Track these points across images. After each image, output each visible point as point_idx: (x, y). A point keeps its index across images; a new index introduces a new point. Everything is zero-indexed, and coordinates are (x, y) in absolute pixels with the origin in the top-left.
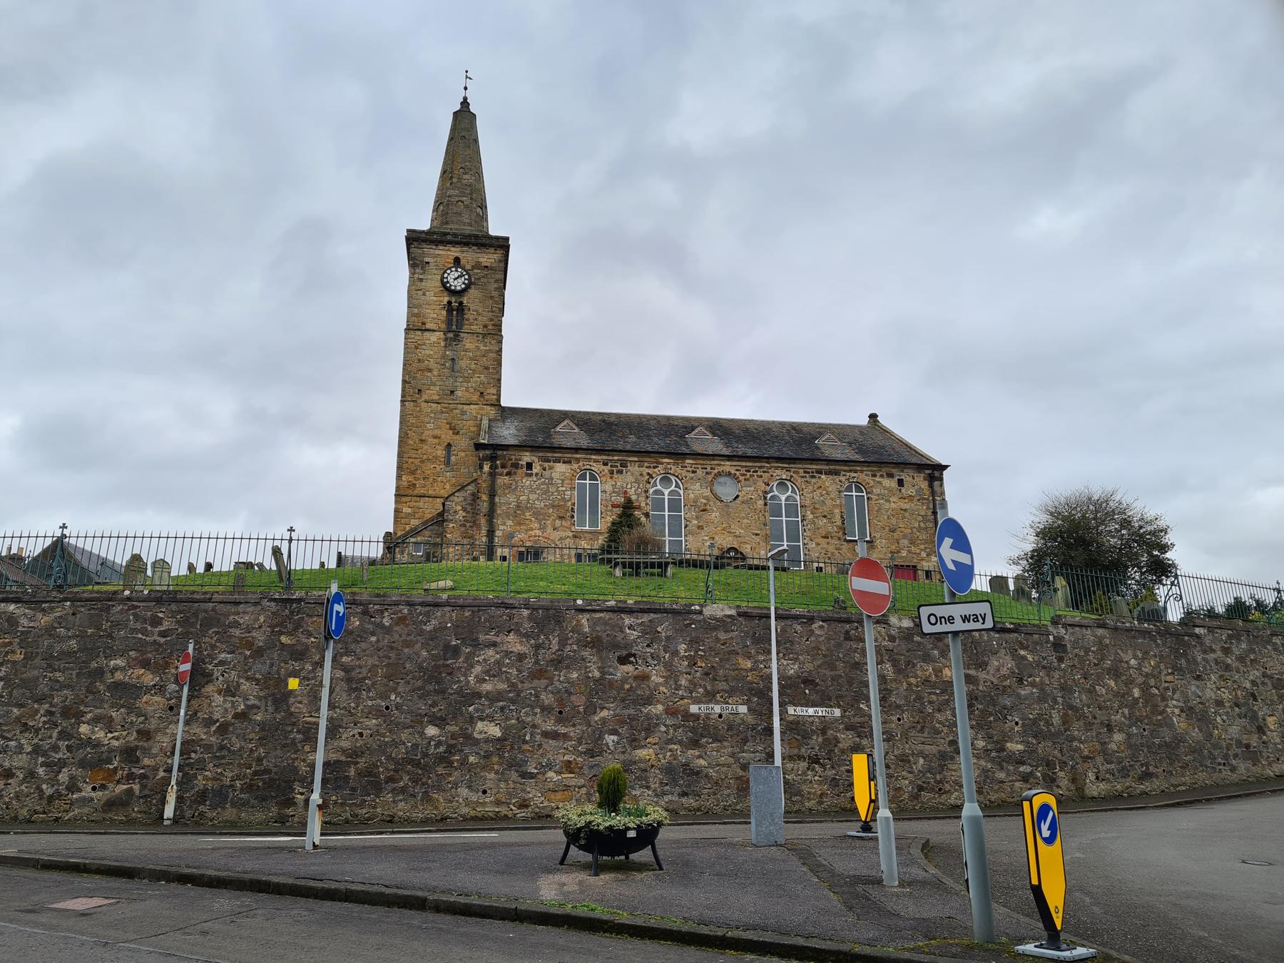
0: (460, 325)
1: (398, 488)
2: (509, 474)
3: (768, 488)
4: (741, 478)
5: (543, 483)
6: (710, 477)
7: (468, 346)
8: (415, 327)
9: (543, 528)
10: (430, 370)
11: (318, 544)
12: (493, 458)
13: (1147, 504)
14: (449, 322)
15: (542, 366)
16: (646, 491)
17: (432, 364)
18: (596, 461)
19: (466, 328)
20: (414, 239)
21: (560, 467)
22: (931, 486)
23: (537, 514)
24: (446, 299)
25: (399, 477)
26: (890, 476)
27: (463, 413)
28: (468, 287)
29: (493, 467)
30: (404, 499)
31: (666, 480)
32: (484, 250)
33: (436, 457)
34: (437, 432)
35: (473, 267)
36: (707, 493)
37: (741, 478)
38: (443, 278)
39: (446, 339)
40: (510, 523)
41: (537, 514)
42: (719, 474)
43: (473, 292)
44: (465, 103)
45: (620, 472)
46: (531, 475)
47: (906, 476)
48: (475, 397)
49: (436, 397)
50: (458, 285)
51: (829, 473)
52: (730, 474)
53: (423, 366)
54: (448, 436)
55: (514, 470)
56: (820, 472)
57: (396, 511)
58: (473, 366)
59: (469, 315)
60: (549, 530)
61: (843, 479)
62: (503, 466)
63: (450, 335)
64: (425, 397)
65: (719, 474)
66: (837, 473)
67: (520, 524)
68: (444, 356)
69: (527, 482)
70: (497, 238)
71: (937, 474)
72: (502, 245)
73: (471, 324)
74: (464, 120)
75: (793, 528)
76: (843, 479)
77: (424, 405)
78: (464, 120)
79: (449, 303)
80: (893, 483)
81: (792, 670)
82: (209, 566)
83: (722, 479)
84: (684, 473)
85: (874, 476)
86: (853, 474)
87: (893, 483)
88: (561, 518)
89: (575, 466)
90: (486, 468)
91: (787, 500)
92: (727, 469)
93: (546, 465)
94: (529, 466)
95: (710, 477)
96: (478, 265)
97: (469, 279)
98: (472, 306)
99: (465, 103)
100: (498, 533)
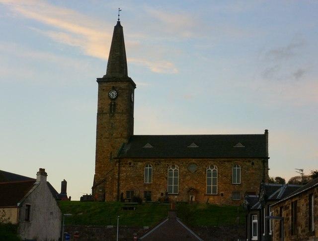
0: (114, 110)
10: (105, 127)
12: (119, 162)
13: (282, 177)
14: (111, 109)
15: (148, 121)
21: (140, 164)
22: (264, 164)
26: (249, 161)
29: (119, 165)
31: (173, 167)
39: (110, 116)
42: (191, 164)
43: (119, 98)
44: (119, 23)
45: (159, 164)
47: (255, 161)
51: (228, 161)
52: (194, 163)
59: (118, 107)
61: (233, 163)
66: (230, 161)
71: (266, 160)
75: (214, 180)
77: (103, 139)
79: (111, 103)
80: (250, 164)
81: (123, 237)
82: (70, 197)
83: (191, 165)
85: (244, 162)
87: (250, 164)
90: (117, 165)
94: (130, 164)
99: (119, 23)
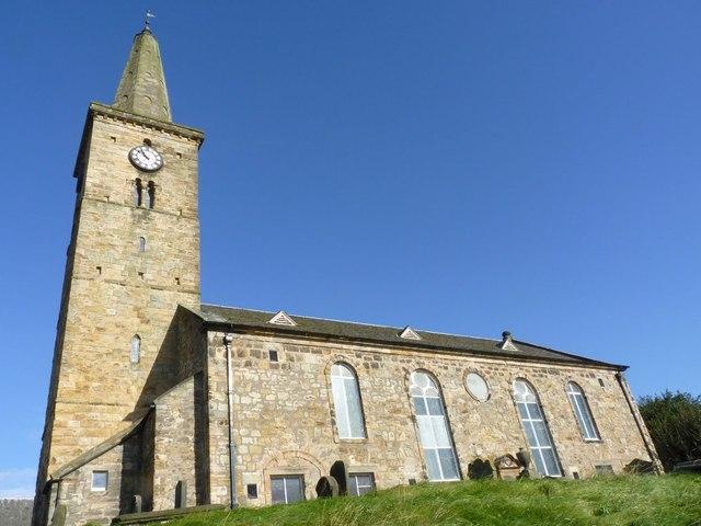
5: (293, 378)
9: (300, 440)
10: (113, 246)
16: (407, 390)
17: (116, 240)
18: (348, 351)
23: (290, 418)
26: (593, 376)
27: (153, 299)
35: (165, 152)
39: (133, 216)
40: (256, 433)
41: (290, 418)
43: (164, 173)
45: (375, 366)
46: (276, 367)
48: (171, 282)
50: (150, 164)
54: (134, 323)
55: (254, 359)
58: (166, 248)
62: (241, 355)
63: (140, 212)
64: (106, 274)
67: (270, 435)
68: (132, 234)
69: (274, 376)
70: (38, 491)
77: (104, 286)
79: (138, 181)
88: (320, 424)
93: (293, 354)
94: (274, 355)
95: (461, 374)
96: (170, 150)
100: (243, 449)
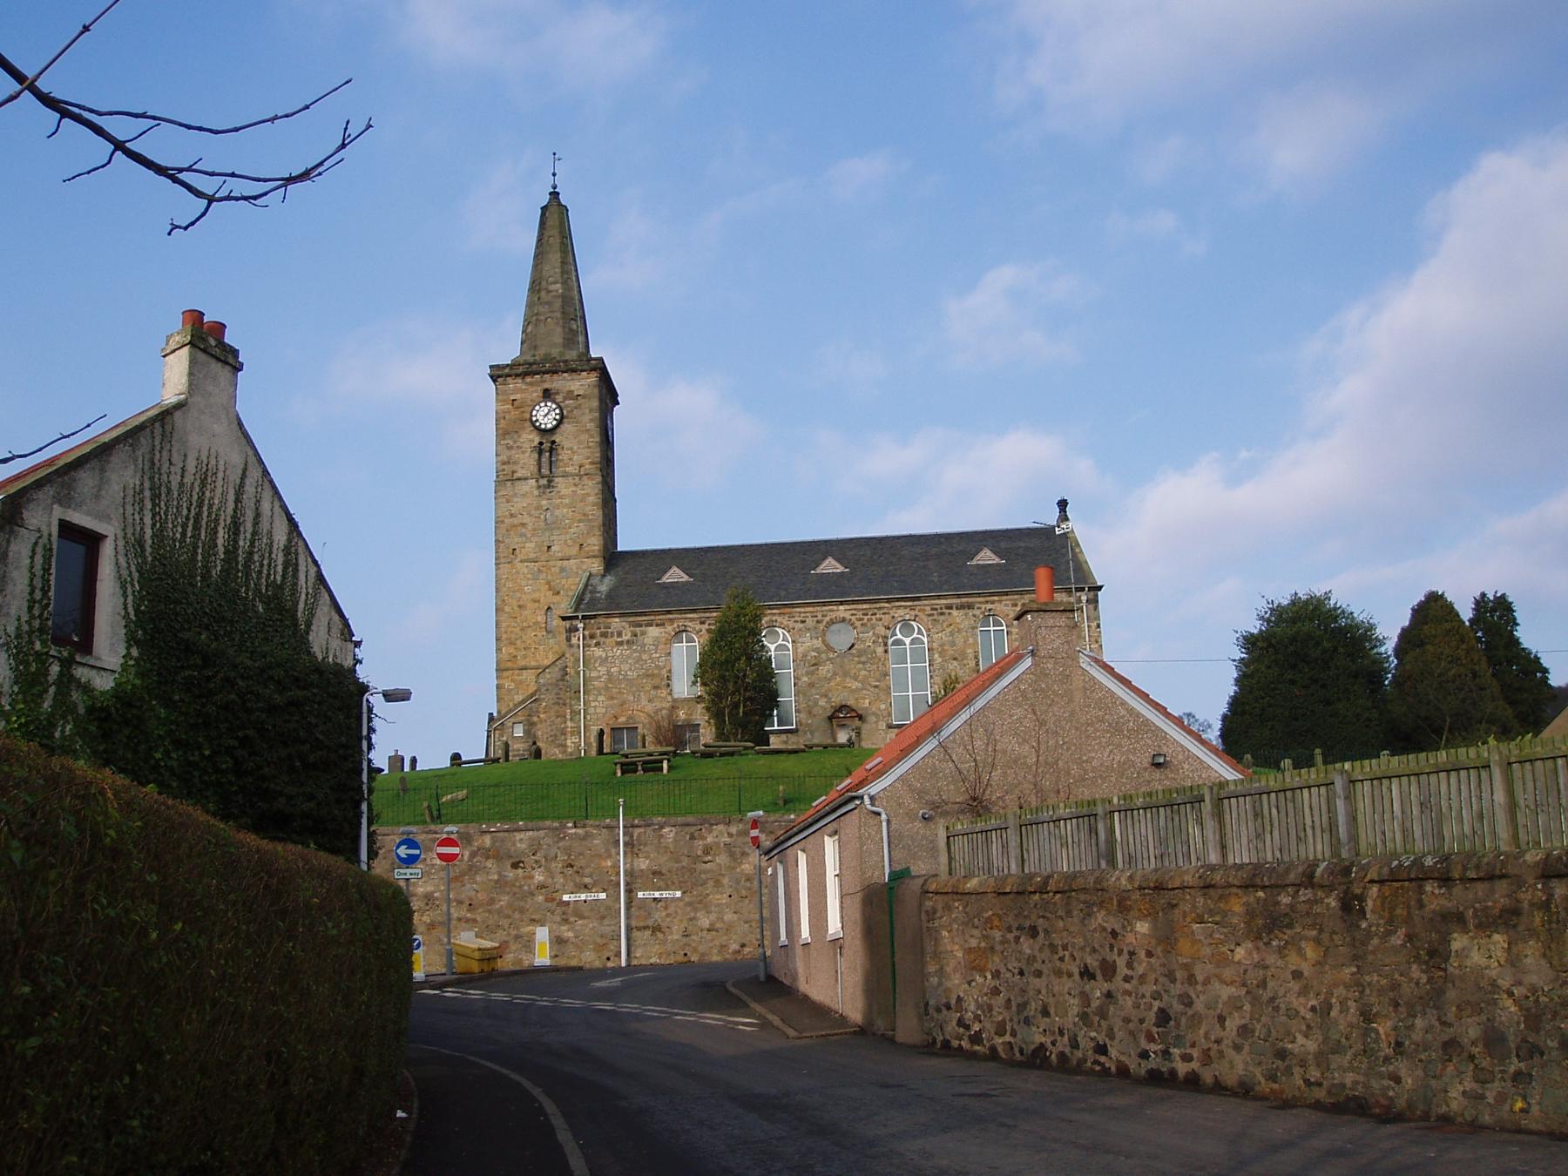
1: (498, 663)
2: (597, 644)
3: (889, 633)
4: (858, 624)
6: (821, 626)
7: (564, 491)
8: (506, 478)
11: (1289, 794)
18: (692, 620)
19: (558, 471)
20: (498, 374)
21: (653, 632)
24: (537, 440)
25: (499, 650)
27: (562, 570)
28: (560, 422)
30: (506, 674)
32: (575, 376)
33: (536, 623)
34: (536, 595)
36: (818, 643)
37: (858, 624)
38: (533, 423)
42: (832, 622)
44: (555, 195)
48: (574, 551)
49: (532, 556)
51: (961, 607)
52: (844, 620)
53: (515, 521)
54: (546, 597)
56: (950, 607)
57: (498, 687)
59: (564, 455)
60: (644, 702)
61: (977, 612)
63: (544, 482)
64: (520, 557)
65: (832, 622)
66: (970, 606)
72: (601, 359)
73: (566, 465)
74: (554, 219)
76: (977, 612)
77: (519, 565)
78: (554, 219)
83: (833, 627)
84: (791, 624)
86: (989, 606)
88: (656, 688)
89: (669, 628)
91: (913, 642)
92: (847, 615)
95: (821, 626)
97: (562, 414)
98: (566, 444)
99: (555, 195)
